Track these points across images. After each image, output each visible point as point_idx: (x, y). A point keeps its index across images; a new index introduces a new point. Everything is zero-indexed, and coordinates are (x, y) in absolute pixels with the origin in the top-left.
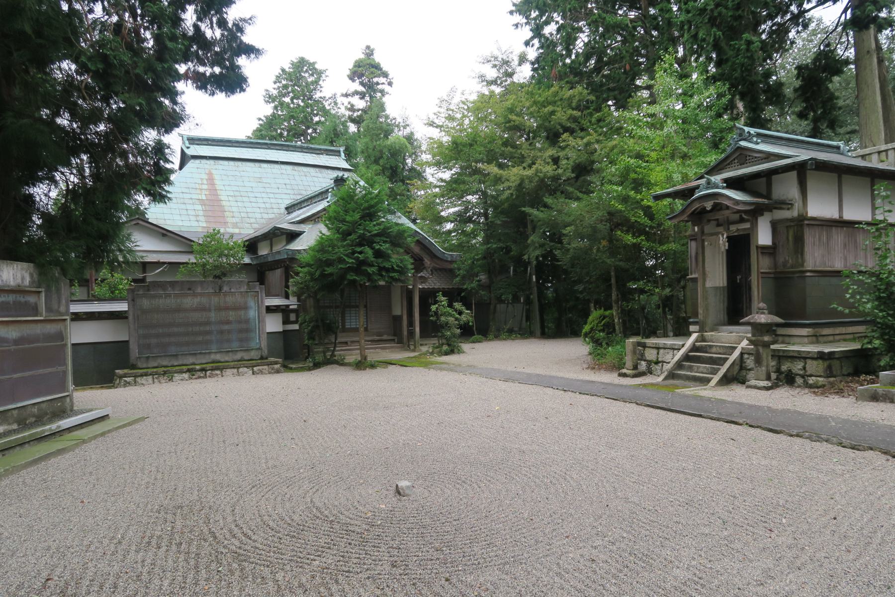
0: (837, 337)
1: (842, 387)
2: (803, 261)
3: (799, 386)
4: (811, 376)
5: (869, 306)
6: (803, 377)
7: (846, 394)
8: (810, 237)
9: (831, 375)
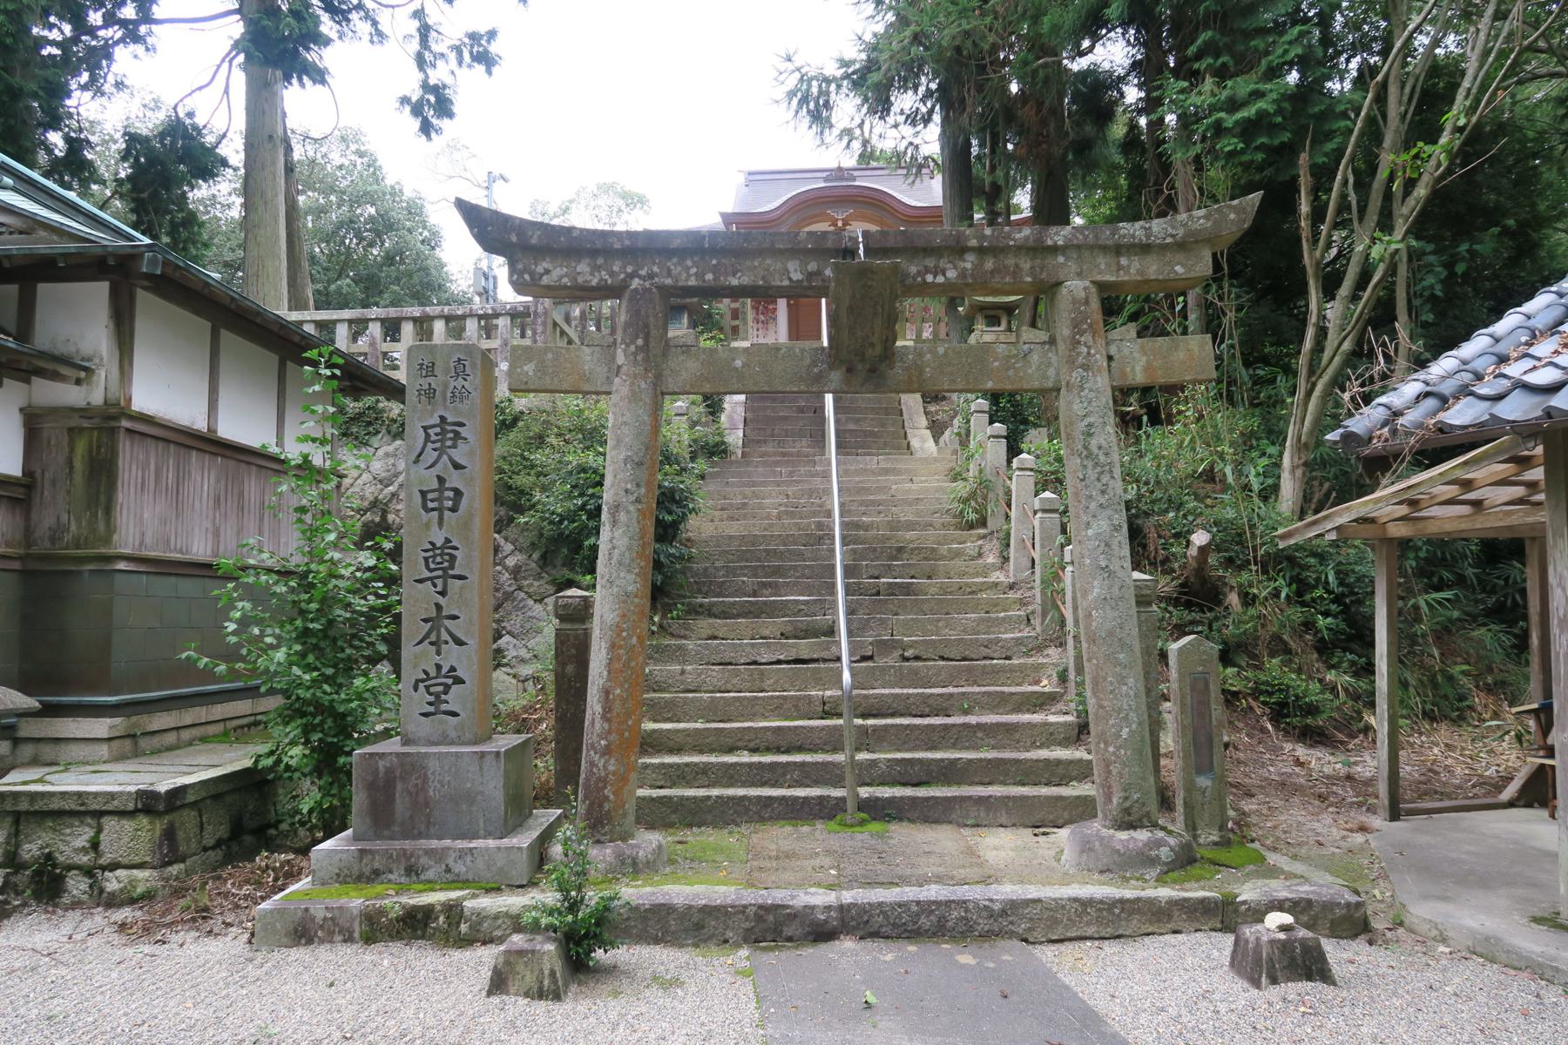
0: (186, 735)
1: (206, 901)
2: (110, 528)
3: (76, 905)
4: (114, 866)
5: (280, 655)
6: (89, 872)
7: (216, 923)
8: (132, 463)
9: (173, 857)
